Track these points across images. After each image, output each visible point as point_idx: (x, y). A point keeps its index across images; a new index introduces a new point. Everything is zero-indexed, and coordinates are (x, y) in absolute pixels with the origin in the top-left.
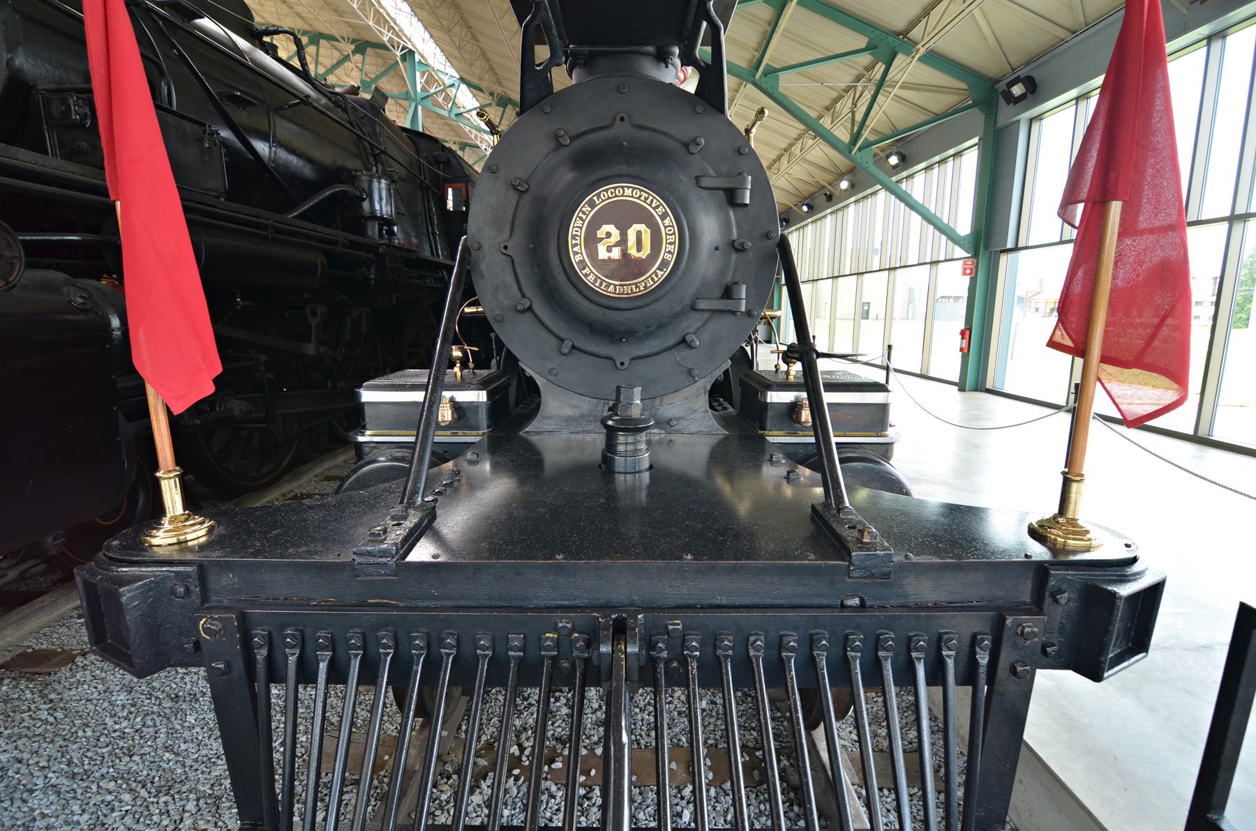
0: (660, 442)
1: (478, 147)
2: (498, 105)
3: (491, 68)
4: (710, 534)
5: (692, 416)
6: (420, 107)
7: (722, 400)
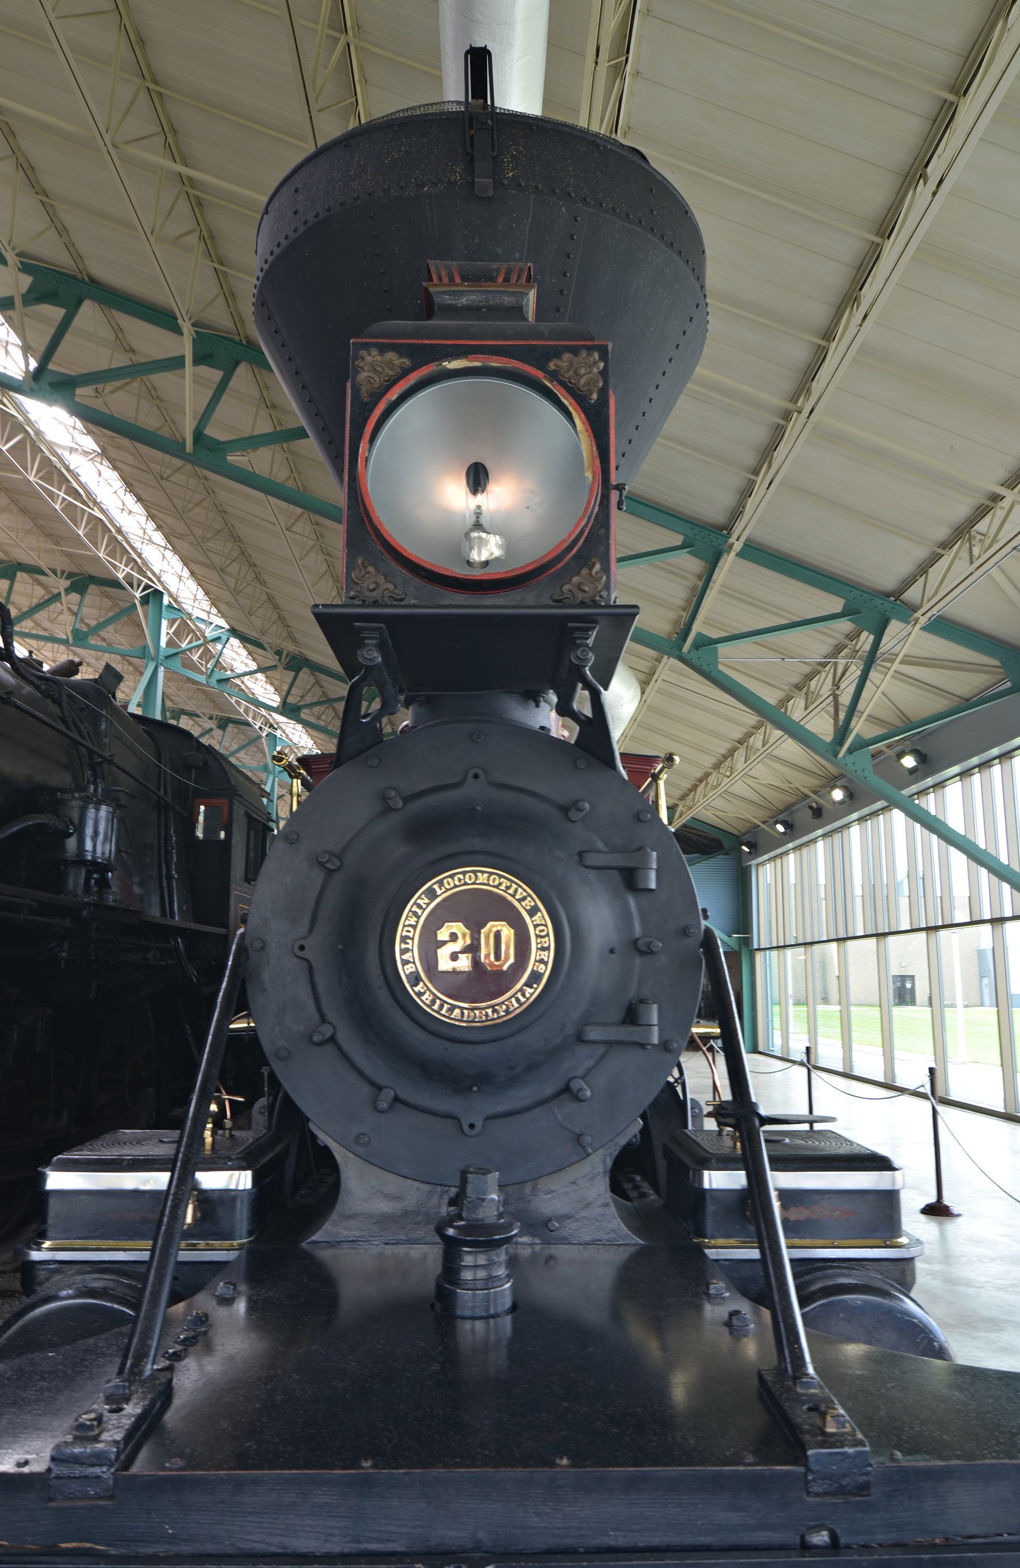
1: (248, 724)
3: (281, 619)
4: (599, 1423)
5: (584, 1214)
6: (161, 669)
7: (638, 1178)
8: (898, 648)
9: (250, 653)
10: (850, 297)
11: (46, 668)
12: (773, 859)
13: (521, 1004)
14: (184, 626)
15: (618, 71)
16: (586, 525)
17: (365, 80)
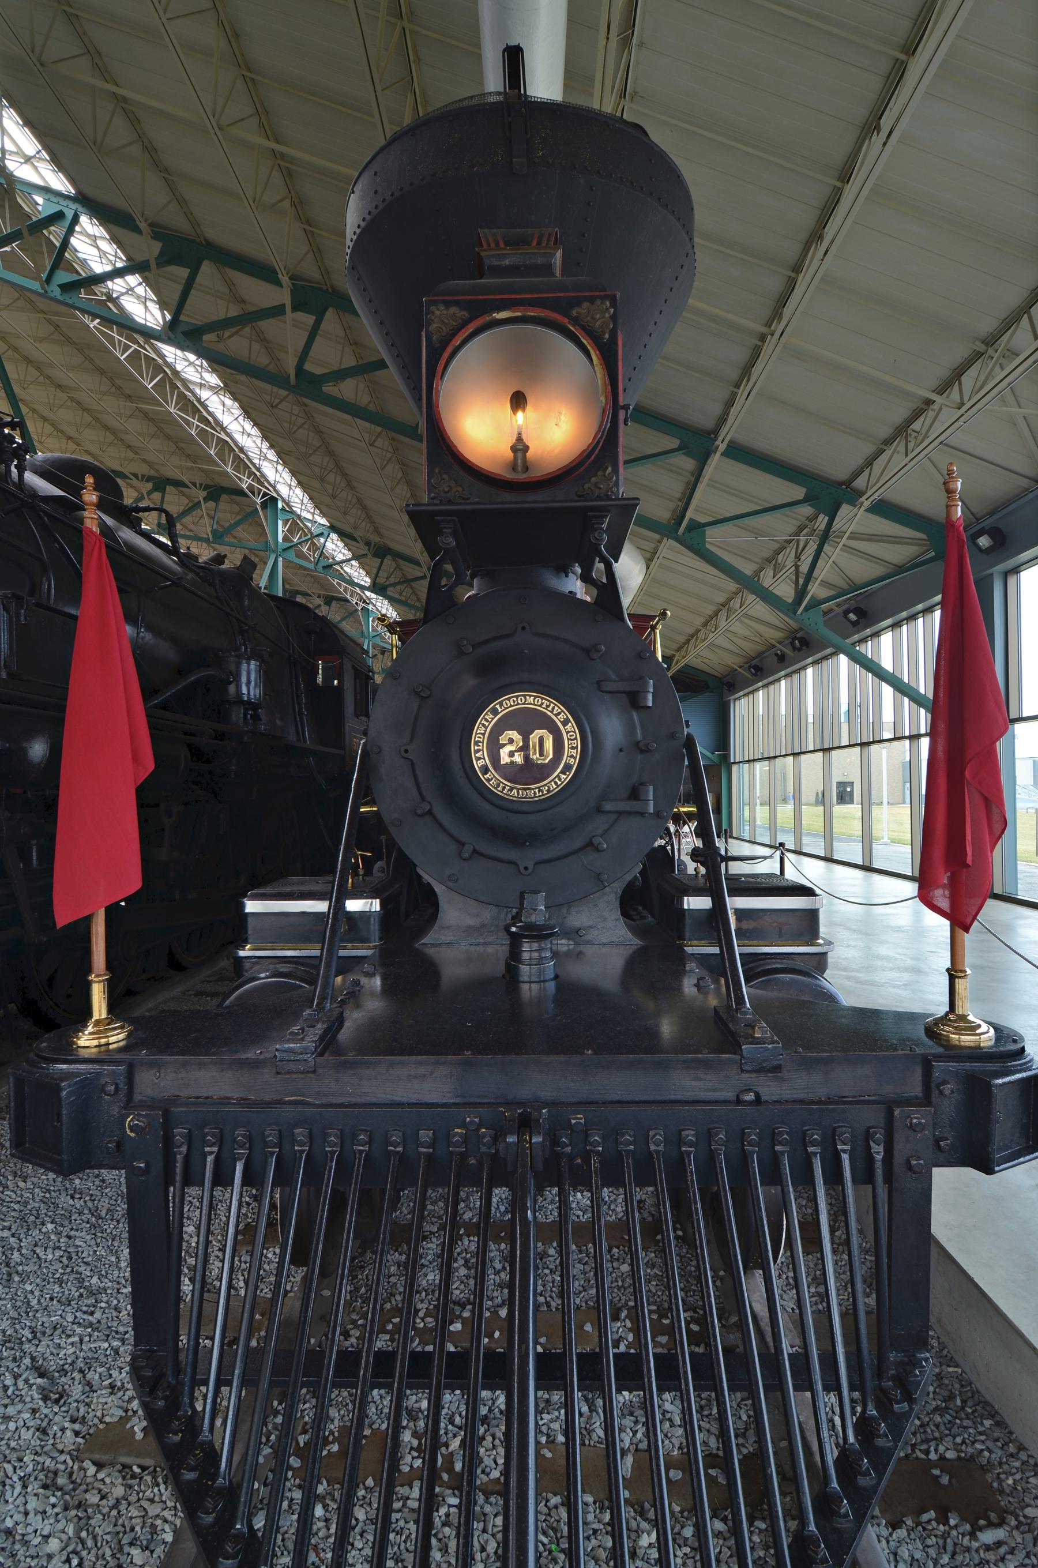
0: (568, 954)
1: (347, 601)
2: (375, 555)
3: (369, 517)
6: (280, 559)
7: (640, 908)
8: (847, 526)
9: (346, 545)
10: (816, 235)
11: (200, 560)
12: (747, 695)
13: (558, 786)
14: (295, 523)
15: (626, 42)
16: (601, 438)
17: (418, 60)
